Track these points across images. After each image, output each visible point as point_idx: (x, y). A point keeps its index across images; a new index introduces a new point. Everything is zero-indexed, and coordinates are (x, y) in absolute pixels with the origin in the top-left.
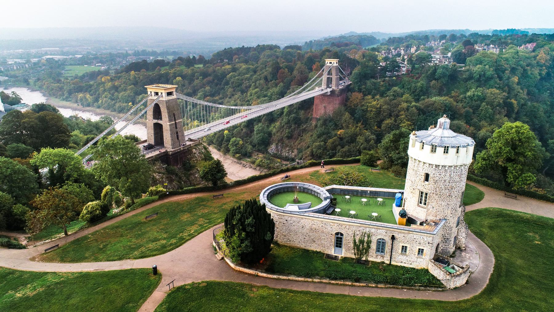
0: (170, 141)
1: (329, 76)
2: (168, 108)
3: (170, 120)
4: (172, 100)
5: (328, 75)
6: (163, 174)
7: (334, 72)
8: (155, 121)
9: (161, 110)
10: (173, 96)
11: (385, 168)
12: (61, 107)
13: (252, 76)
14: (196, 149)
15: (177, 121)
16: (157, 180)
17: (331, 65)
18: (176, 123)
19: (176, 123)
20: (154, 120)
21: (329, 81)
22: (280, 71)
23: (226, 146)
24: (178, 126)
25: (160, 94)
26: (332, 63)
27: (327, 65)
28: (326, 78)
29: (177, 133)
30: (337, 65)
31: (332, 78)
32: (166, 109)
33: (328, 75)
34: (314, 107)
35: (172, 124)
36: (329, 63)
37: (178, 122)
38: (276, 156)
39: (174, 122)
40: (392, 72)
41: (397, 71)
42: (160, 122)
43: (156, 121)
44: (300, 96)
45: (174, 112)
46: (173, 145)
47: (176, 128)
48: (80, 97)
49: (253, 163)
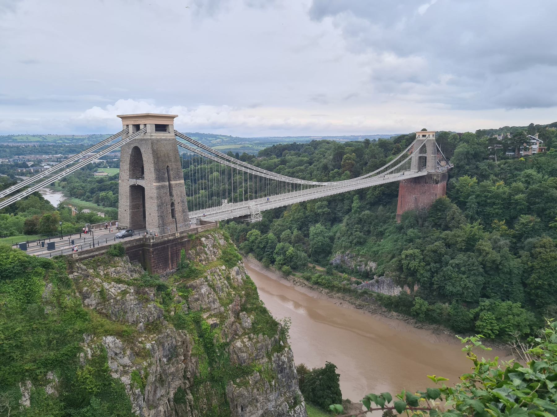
0: (157, 218)
1: (421, 155)
2: (156, 155)
3: (159, 178)
4: (165, 140)
5: (420, 153)
6: (128, 285)
7: (430, 149)
8: (133, 182)
9: (144, 159)
10: (168, 134)
11: (525, 292)
12: (263, 290)
13: (307, 167)
14: (207, 238)
15: (172, 182)
16: (111, 298)
17: (424, 138)
18: (170, 185)
19: (170, 185)
20: (131, 180)
21: (423, 162)
22: (345, 156)
23: (270, 255)
24: (174, 193)
25: (142, 127)
26: (427, 136)
27: (419, 139)
28: (417, 158)
29: (173, 204)
30: (434, 138)
31: (426, 157)
32: (151, 155)
33: (420, 153)
34: (399, 198)
35: (163, 187)
36: (421, 136)
37: (176, 184)
38: (340, 268)
39: (167, 183)
40: (516, 151)
41: (526, 149)
42: (140, 182)
43: (134, 180)
44: (281, 282)
45: (169, 164)
46: (163, 225)
47: (171, 195)
48: (102, 195)
49: (308, 279)
